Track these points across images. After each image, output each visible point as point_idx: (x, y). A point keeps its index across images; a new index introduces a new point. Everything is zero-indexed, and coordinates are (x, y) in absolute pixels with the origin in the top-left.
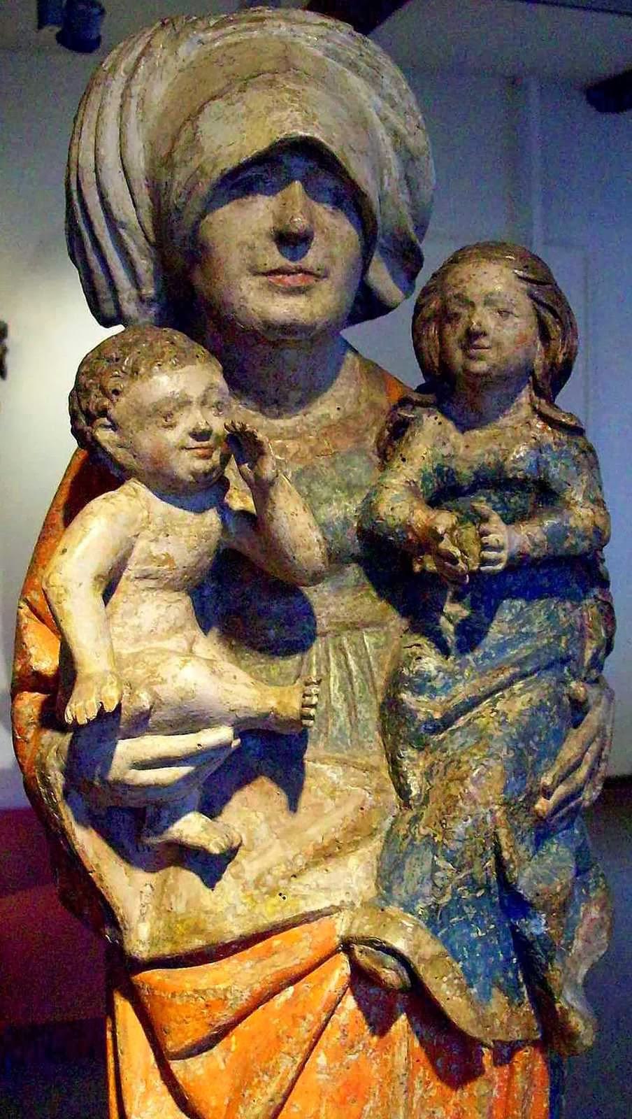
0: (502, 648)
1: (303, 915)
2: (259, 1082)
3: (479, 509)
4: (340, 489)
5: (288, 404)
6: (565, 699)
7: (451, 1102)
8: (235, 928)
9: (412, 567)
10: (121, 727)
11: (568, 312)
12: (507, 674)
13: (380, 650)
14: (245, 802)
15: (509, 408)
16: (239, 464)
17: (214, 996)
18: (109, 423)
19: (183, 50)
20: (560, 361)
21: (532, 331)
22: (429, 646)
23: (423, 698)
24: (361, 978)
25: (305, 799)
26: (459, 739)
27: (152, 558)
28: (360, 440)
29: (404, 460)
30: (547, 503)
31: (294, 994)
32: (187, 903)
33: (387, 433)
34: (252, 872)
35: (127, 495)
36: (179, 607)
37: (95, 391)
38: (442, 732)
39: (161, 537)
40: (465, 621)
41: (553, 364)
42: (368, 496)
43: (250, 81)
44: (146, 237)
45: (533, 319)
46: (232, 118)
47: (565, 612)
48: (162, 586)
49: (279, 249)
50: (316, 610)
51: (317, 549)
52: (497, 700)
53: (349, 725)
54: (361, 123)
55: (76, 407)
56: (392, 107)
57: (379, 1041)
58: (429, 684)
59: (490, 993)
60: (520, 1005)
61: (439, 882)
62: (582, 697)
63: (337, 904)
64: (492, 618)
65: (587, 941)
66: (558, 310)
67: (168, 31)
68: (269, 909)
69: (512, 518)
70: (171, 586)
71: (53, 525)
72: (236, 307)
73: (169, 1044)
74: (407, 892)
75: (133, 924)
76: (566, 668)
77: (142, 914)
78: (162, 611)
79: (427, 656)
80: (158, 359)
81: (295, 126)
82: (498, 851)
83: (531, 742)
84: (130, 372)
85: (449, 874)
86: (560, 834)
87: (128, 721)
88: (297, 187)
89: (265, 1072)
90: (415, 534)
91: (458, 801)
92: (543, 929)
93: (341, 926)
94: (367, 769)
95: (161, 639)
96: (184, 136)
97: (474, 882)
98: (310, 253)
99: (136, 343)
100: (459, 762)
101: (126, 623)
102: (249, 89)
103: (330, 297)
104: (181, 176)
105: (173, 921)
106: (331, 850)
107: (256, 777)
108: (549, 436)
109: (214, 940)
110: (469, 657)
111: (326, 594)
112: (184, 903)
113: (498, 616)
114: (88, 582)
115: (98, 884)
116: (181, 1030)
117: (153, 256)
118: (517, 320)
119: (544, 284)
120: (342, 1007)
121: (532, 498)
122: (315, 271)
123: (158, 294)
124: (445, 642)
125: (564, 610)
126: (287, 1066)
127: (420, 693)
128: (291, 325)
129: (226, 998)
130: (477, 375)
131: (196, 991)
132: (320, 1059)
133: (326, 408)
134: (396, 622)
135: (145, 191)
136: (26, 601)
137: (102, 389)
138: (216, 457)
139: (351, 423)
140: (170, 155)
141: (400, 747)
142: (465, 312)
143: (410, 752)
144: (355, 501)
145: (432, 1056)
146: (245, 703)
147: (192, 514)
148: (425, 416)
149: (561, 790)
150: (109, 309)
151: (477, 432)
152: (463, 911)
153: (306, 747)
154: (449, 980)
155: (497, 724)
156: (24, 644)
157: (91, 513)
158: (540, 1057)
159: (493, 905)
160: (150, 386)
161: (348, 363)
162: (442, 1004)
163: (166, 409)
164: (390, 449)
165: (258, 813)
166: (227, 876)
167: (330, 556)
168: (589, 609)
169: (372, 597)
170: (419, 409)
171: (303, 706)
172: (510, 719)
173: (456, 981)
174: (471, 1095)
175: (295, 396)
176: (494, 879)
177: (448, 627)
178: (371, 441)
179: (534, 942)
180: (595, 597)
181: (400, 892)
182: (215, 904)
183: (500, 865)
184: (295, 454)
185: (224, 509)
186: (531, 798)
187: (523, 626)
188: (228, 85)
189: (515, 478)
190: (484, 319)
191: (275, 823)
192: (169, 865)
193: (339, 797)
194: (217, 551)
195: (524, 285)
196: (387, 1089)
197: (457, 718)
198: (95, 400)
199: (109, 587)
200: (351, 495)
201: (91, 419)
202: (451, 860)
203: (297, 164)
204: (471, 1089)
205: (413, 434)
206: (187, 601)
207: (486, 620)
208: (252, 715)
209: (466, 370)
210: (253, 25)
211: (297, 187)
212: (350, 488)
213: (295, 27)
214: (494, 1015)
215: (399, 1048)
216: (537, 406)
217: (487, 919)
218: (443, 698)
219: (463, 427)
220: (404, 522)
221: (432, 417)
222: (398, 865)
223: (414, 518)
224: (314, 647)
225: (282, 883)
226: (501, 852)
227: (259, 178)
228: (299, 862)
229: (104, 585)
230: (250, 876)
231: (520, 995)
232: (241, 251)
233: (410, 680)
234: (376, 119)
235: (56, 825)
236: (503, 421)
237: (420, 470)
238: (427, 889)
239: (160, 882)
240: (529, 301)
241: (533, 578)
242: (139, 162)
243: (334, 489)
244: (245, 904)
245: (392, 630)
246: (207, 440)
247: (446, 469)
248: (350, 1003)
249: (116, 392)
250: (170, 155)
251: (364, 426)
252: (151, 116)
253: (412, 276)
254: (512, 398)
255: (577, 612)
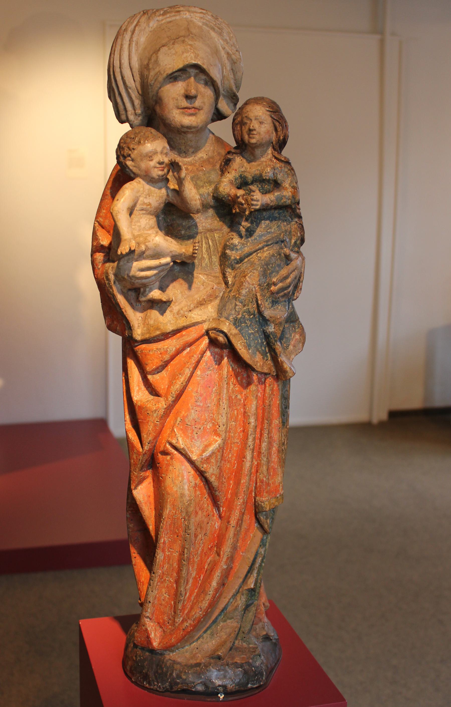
0: (260, 236)
1: (193, 323)
2: (178, 377)
3: (251, 188)
4: (207, 182)
5: (189, 153)
6: (282, 254)
7: (243, 394)
8: (170, 328)
9: (232, 211)
10: (135, 257)
11: (285, 122)
12: (262, 245)
13: (220, 239)
14: (174, 287)
15: (264, 155)
16: (173, 172)
17: (163, 350)
18: (131, 159)
19: (151, 24)
20: (281, 139)
21: (272, 129)
22: (236, 235)
23: (234, 252)
24: (213, 342)
25: (194, 286)
26: (245, 265)
27: (144, 204)
28: (214, 166)
29: (229, 173)
30: (277, 187)
31: (190, 350)
32: (154, 321)
33: (223, 163)
34: (176, 310)
35: (137, 182)
36: (152, 221)
37: (126, 149)
38: (240, 264)
39: (147, 197)
40: (249, 228)
41: (279, 140)
42: (216, 185)
43: (177, 40)
44: (138, 92)
45: (272, 124)
46: (170, 55)
47: (284, 226)
48: (147, 213)
49: (186, 100)
50: (198, 225)
51: (198, 201)
52: (258, 253)
53: (209, 263)
54: (216, 52)
55: (119, 153)
56: (227, 44)
57: (218, 367)
58: (235, 247)
59: (256, 354)
60: (267, 360)
61: (237, 310)
62: (288, 254)
63: (204, 319)
64: (258, 227)
65: (294, 346)
66: (280, 121)
67: (146, 16)
68: (182, 321)
69: (265, 192)
70: (150, 214)
71: (107, 195)
72: (172, 120)
73: (148, 368)
74: (227, 314)
75: (136, 329)
76: (283, 244)
77: (139, 326)
78: (147, 221)
79: (235, 238)
80: (147, 138)
81: (192, 59)
82: (257, 301)
83: (269, 266)
84: (138, 142)
85: (241, 307)
86: (282, 303)
87: (137, 255)
88: (192, 78)
89: (180, 374)
90: (231, 197)
91: (243, 283)
92: (273, 330)
93: (206, 326)
94: (216, 277)
95: (147, 230)
96: (153, 59)
97: (249, 312)
98: (197, 102)
99: (139, 133)
100: (244, 271)
101: (136, 225)
102: (176, 44)
103: (203, 116)
104: (152, 73)
105: (149, 327)
106: (202, 302)
107: (178, 279)
108: (278, 165)
109: (164, 331)
110: (250, 239)
111: (202, 219)
112: (153, 321)
113: (260, 226)
114: (125, 210)
115: (125, 313)
116: (152, 363)
117: (141, 99)
118: (266, 125)
119: (276, 112)
120: (206, 355)
121: (272, 186)
122: (198, 108)
123: (142, 113)
124: (241, 234)
125: (284, 225)
126: (188, 372)
127: (233, 250)
128: (190, 126)
129: (167, 351)
130: (253, 144)
131: (157, 349)
132: (198, 372)
133: (202, 155)
134: (226, 229)
135: (138, 75)
136: (97, 221)
137: (129, 148)
138: (166, 170)
139: (211, 160)
140: (148, 65)
141: (226, 268)
142: (248, 122)
143: (229, 270)
144: (212, 187)
145: (237, 375)
146: (175, 249)
147: (157, 190)
148: (236, 158)
149: (280, 285)
150: (123, 117)
151: (253, 163)
152: (246, 322)
153: (194, 270)
154: (240, 343)
155: (257, 260)
156: (97, 236)
157: (126, 188)
158: (276, 384)
159: (256, 321)
160: (145, 147)
161: (210, 138)
162: (238, 350)
163: (150, 155)
164: (224, 169)
165: (178, 291)
166: (168, 312)
167: (203, 206)
168: (294, 225)
169: (218, 221)
170: (235, 155)
171: (193, 250)
172: (262, 258)
173: (243, 344)
174: (250, 390)
175: (191, 150)
176: (256, 312)
177: (242, 230)
178: (218, 166)
179: (270, 334)
180: (296, 222)
181: (225, 314)
182: (164, 320)
183: (258, 306)
184: (191, 170)
185: (167, 188)
186: (269, 285)
187: (268, 229)
188: (168, 41)
189: (266, 179)
190: (255, 125)
191: (184, 293)
192: (147, 310)
193: (205, 285)
194: (165, 202)
195: (268, 113)
196: (220, 383)
197: (245, 259)
198: (126, 151)
199: (131, 212)
200: (210, 185)
201: (125, 157)
202: (242, 303)
203: (193, 71)
204: (250, 388)
205: (232, 164)
206: (155, 219)
207: (256, 227)
208: (177, 254)
209: (249, 142)
210: (176, 14)
211: (192, 78)
212: (210, 182)
213: (192, 15)
214: (257, 361)
215: (225, 369)
216: (274, 154)
217: (254, 326)
218: (240, 252)
219: (249, 161)
220: (228, 193)
221: (239, 158)
222: (224, 306)
223: (231, 192)
224: (197, 237)
225: (186, 313)
226: (258, 301)
227: (179, 76)
228: (192, 306)
229: (130, 212)
230: (175, 311)
231: (267, 356)
232: (173, 101)
233: (229, 246)
234: (221, 48)
235: (111, 294)
236: (262, 159)
237: (234, 176)
238: (233, 312)
239: (144, 316)
240: (270, 119)
241: (273, 214)
242: (136, 64)
243: (205, 183)
244: (174, 320)
245: (224, 232)
246: (163, 164)
247: (243, 176)
248: (208, 353)
249: (134, 149)
250: (148, 65)
251: (216, 161)
252: (140, 49)
253: (235, 105)
254: (266, 151)
255: (289, 226)
